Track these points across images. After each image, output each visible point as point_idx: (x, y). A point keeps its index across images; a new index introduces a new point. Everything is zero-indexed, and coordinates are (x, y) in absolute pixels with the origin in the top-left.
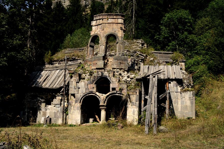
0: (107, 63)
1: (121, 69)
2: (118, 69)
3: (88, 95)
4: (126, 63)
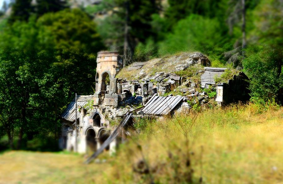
1: (111, 106)
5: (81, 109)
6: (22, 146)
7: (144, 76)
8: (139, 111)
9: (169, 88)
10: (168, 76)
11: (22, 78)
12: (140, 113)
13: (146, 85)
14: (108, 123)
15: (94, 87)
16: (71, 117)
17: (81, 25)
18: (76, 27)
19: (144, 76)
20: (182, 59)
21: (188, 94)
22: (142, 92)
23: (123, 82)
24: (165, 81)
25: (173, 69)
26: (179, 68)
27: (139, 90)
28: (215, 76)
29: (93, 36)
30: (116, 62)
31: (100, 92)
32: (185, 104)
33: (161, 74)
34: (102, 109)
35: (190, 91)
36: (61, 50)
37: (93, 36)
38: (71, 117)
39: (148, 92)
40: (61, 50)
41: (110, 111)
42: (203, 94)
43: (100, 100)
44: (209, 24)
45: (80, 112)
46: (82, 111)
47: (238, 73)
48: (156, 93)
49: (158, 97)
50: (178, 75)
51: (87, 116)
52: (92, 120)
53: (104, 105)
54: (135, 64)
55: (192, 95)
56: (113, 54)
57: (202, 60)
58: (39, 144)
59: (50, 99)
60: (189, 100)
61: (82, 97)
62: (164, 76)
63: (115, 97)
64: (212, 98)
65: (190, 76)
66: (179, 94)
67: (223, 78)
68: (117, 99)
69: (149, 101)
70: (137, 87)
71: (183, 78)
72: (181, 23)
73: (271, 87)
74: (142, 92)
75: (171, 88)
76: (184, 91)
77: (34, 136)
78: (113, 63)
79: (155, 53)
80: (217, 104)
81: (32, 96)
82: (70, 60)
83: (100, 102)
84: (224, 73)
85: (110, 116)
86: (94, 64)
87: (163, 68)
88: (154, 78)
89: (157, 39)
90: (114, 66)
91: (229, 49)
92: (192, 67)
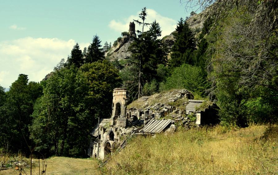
1: (121, 126)
5: (102, 128)
6: (65, 153)
7: (147, 106)
8: (140, 130)
9: (163, 114)
10: (163, 106)
11: (64, 106)
12: (141, 132)
13: (148, 112)
14: (119, 138)
15: (111, 113)
16: (96, 134)
17: (108, 71)
18: (104, 72)
19: (147, 106)
20: (173, 94)
21: (176, 118)
22: (145, 116)
23: (134, 110)
24: (161, 109)
25: (167, 101)
26: (171, 100)
27: (143, 115)
28: (194, 106)
29: (116, 78)
30: (126, 96)
31: (114, 116)
32: (173, 125)
33: (158, 104)
34: (115, 128)
35: (178, 116)
36: (94, 88)
37: (116, 78)
38: (96, 134)
39: (148, 117)
40: (94, 88)
41: (120, 130)
42: (186, 118)
43: (114, 122)
44: (195, 70)
45: (101, 130)
46: (103, 129)
47: (212, 104)
48: (154, 117)
49: (155, 121)
50: (169, 105)
51: (106, 133)
52: (108, 136)
53: (117, 125)
54: (143, 97)
55: (179, 119)
56: (123, 90)
57: (187, 95)
58: (77, 152)
59: (82, 121)
60: (176, 123)
61: (104, 119)
62: (160, 106)
63: (124, 120)
64: (193, 121)
65: (178, 106)
66: (170, 119)
67: (201, 107)
68: (126, 121)
69: (149, 123)
70: (141, 113)
71: (173, 107)
72: (177, 69)
73: (234, 115)
74: (145, 117)
75: (164, 114)
76: (173, 117)
77: (74, 146)
78: (123, 96)
79: (157, 90)
80: (196, 126)
81: (70, 118)
82: (100, 94)
83: (114, 123)
84: (202, 104)
85: (120, 134)
86: (111, 98)
87: (160, 100)
88: (153, 107)
89: (159, 79)
90: (124, 99)
91: (208, 88)
92: (180, 99)
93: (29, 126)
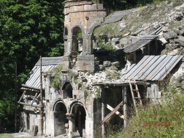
0: (75, 63)
1: (85, 71)
2: (82, 71)
3: (59, 102)
4: (91, 64)
43: (70, 63)
93: (39, 40)
